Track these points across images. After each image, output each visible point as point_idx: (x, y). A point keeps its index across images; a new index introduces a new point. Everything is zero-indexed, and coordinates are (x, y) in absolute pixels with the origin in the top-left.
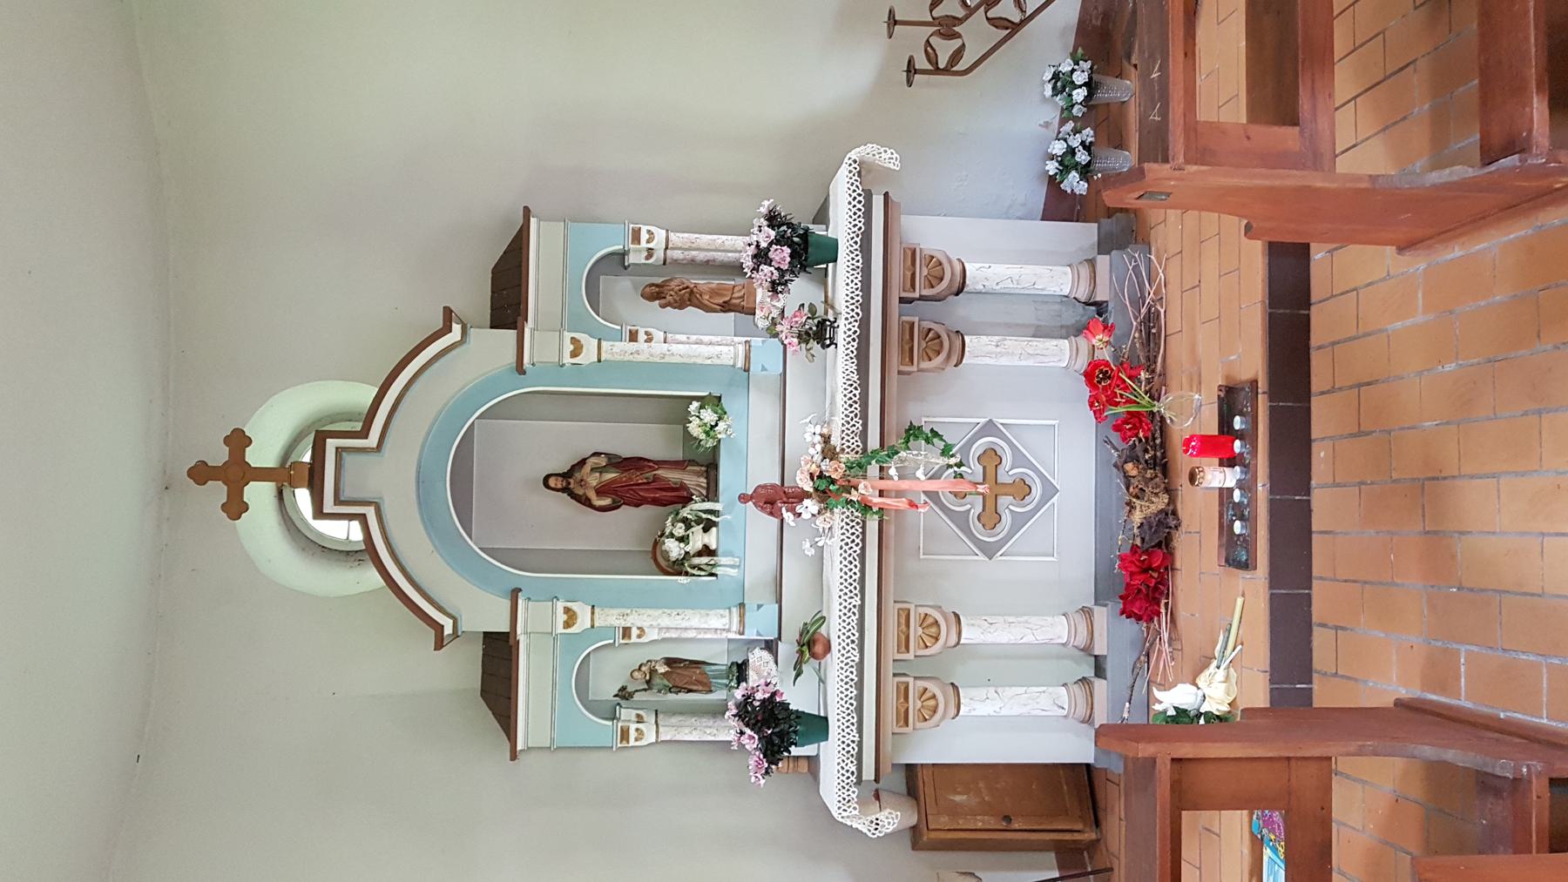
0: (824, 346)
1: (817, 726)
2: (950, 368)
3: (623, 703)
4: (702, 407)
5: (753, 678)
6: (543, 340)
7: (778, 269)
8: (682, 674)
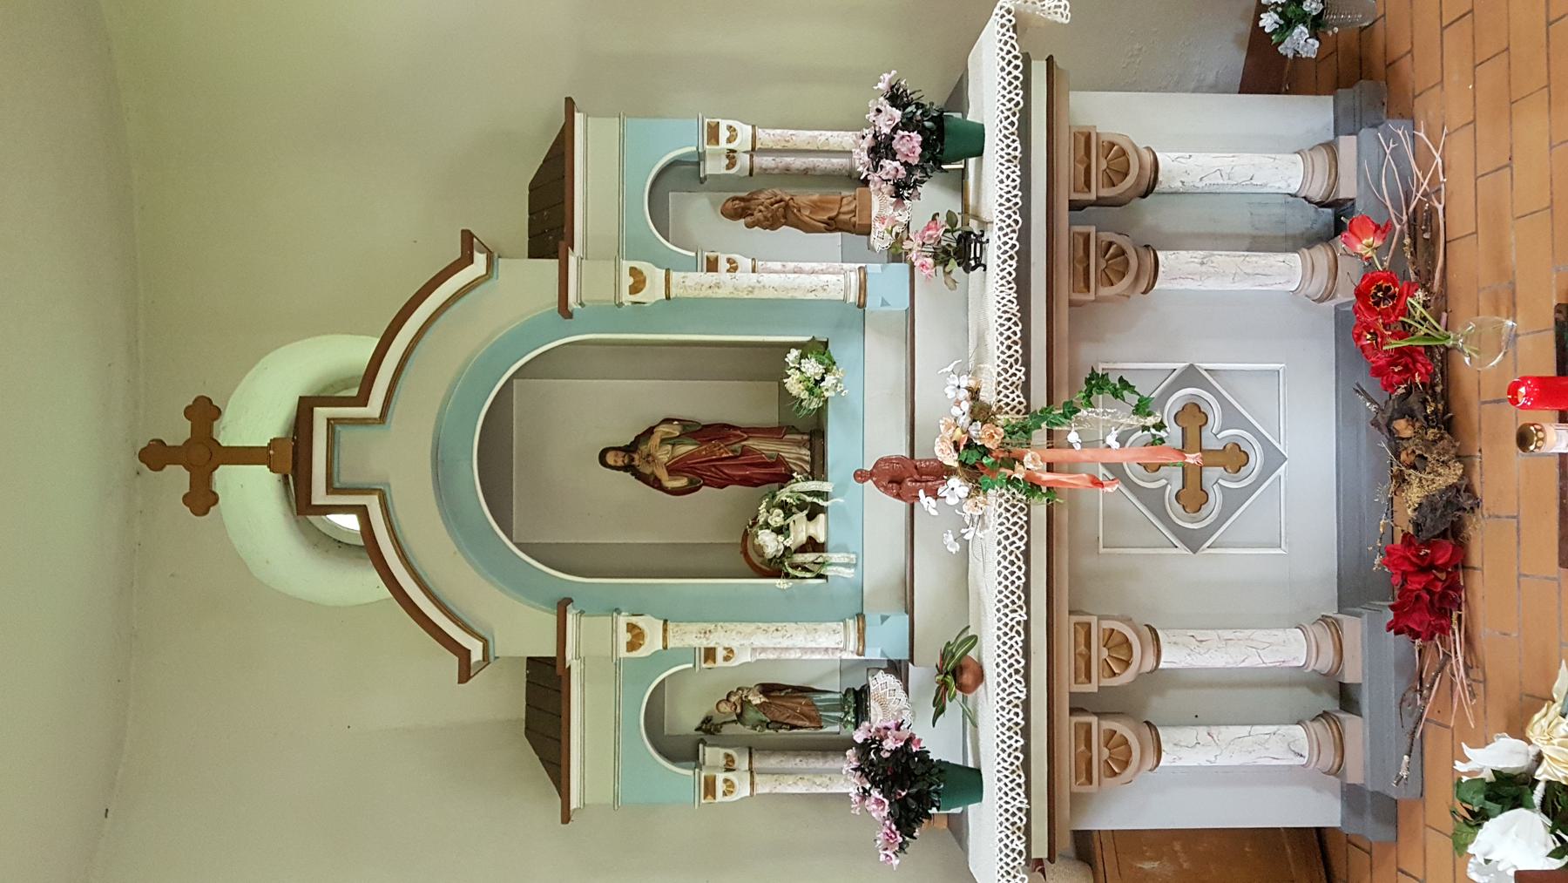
0: (968, 269)
1: (968, 782)
2: (1137, 295)
3: (707, 738)
4: (803, 356)
5: (878, 717)
6: (592, 273)
7: (905, 164)
8: (781, 715)
